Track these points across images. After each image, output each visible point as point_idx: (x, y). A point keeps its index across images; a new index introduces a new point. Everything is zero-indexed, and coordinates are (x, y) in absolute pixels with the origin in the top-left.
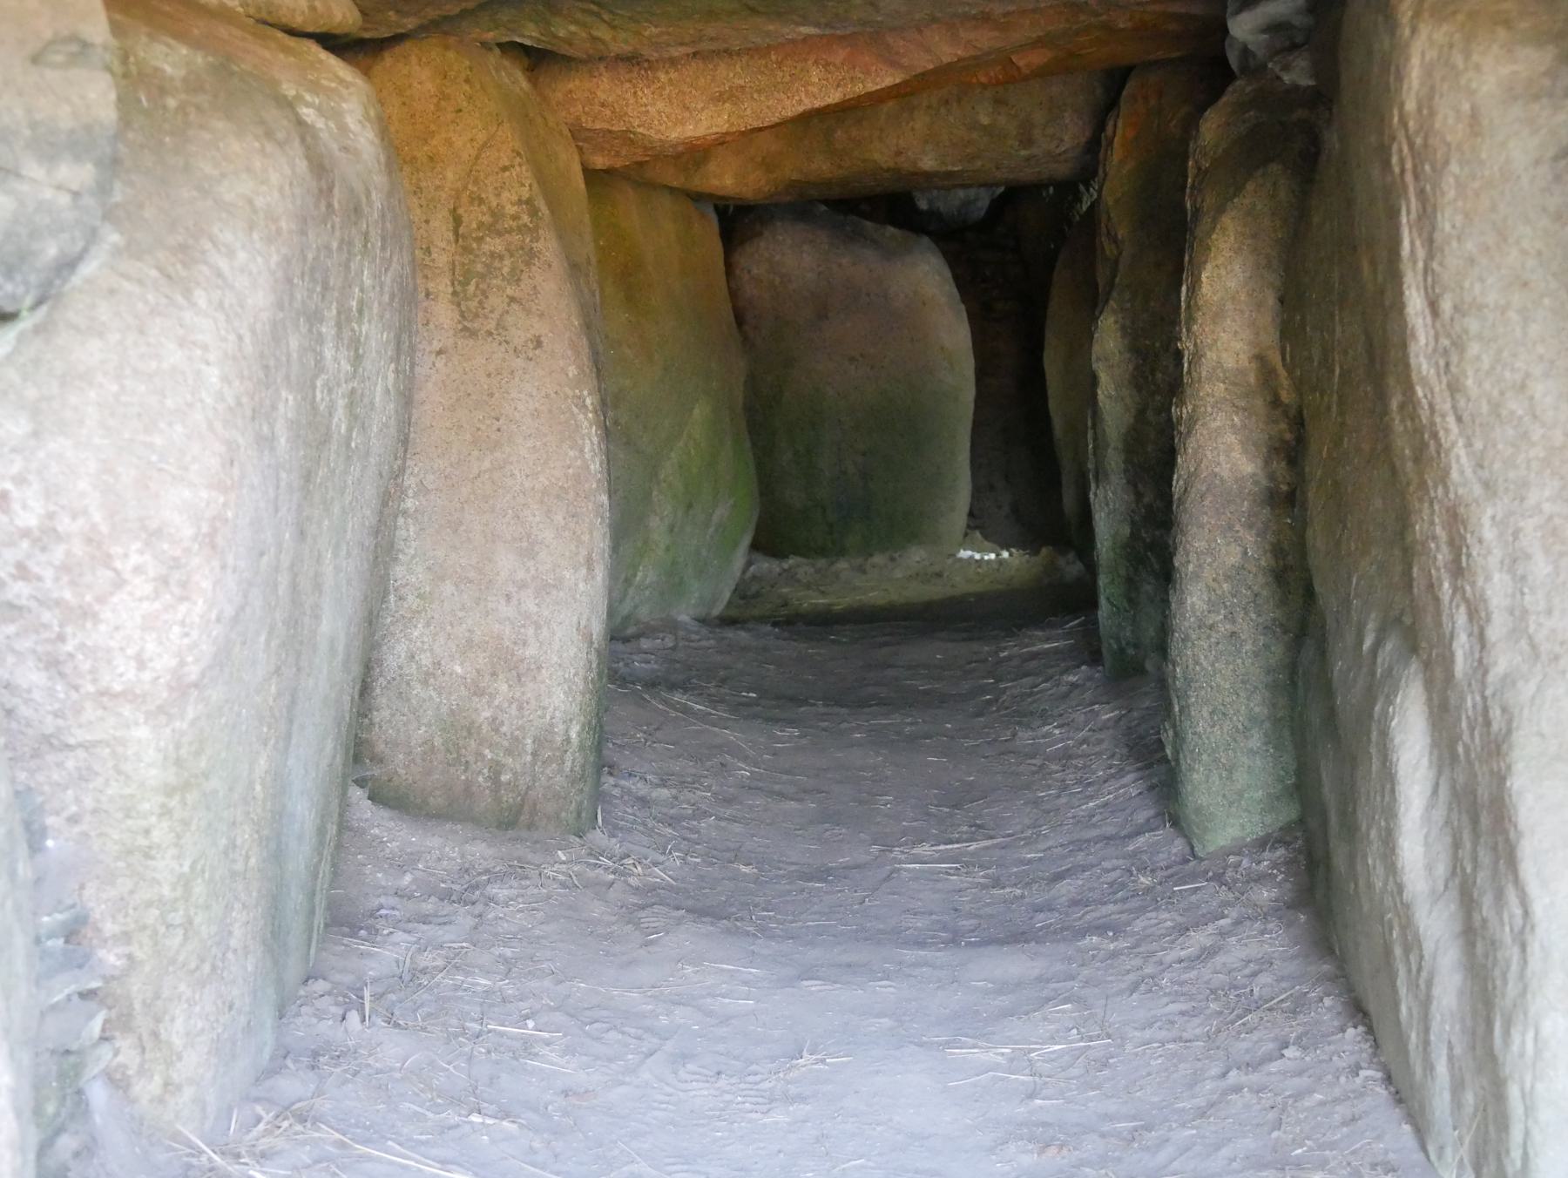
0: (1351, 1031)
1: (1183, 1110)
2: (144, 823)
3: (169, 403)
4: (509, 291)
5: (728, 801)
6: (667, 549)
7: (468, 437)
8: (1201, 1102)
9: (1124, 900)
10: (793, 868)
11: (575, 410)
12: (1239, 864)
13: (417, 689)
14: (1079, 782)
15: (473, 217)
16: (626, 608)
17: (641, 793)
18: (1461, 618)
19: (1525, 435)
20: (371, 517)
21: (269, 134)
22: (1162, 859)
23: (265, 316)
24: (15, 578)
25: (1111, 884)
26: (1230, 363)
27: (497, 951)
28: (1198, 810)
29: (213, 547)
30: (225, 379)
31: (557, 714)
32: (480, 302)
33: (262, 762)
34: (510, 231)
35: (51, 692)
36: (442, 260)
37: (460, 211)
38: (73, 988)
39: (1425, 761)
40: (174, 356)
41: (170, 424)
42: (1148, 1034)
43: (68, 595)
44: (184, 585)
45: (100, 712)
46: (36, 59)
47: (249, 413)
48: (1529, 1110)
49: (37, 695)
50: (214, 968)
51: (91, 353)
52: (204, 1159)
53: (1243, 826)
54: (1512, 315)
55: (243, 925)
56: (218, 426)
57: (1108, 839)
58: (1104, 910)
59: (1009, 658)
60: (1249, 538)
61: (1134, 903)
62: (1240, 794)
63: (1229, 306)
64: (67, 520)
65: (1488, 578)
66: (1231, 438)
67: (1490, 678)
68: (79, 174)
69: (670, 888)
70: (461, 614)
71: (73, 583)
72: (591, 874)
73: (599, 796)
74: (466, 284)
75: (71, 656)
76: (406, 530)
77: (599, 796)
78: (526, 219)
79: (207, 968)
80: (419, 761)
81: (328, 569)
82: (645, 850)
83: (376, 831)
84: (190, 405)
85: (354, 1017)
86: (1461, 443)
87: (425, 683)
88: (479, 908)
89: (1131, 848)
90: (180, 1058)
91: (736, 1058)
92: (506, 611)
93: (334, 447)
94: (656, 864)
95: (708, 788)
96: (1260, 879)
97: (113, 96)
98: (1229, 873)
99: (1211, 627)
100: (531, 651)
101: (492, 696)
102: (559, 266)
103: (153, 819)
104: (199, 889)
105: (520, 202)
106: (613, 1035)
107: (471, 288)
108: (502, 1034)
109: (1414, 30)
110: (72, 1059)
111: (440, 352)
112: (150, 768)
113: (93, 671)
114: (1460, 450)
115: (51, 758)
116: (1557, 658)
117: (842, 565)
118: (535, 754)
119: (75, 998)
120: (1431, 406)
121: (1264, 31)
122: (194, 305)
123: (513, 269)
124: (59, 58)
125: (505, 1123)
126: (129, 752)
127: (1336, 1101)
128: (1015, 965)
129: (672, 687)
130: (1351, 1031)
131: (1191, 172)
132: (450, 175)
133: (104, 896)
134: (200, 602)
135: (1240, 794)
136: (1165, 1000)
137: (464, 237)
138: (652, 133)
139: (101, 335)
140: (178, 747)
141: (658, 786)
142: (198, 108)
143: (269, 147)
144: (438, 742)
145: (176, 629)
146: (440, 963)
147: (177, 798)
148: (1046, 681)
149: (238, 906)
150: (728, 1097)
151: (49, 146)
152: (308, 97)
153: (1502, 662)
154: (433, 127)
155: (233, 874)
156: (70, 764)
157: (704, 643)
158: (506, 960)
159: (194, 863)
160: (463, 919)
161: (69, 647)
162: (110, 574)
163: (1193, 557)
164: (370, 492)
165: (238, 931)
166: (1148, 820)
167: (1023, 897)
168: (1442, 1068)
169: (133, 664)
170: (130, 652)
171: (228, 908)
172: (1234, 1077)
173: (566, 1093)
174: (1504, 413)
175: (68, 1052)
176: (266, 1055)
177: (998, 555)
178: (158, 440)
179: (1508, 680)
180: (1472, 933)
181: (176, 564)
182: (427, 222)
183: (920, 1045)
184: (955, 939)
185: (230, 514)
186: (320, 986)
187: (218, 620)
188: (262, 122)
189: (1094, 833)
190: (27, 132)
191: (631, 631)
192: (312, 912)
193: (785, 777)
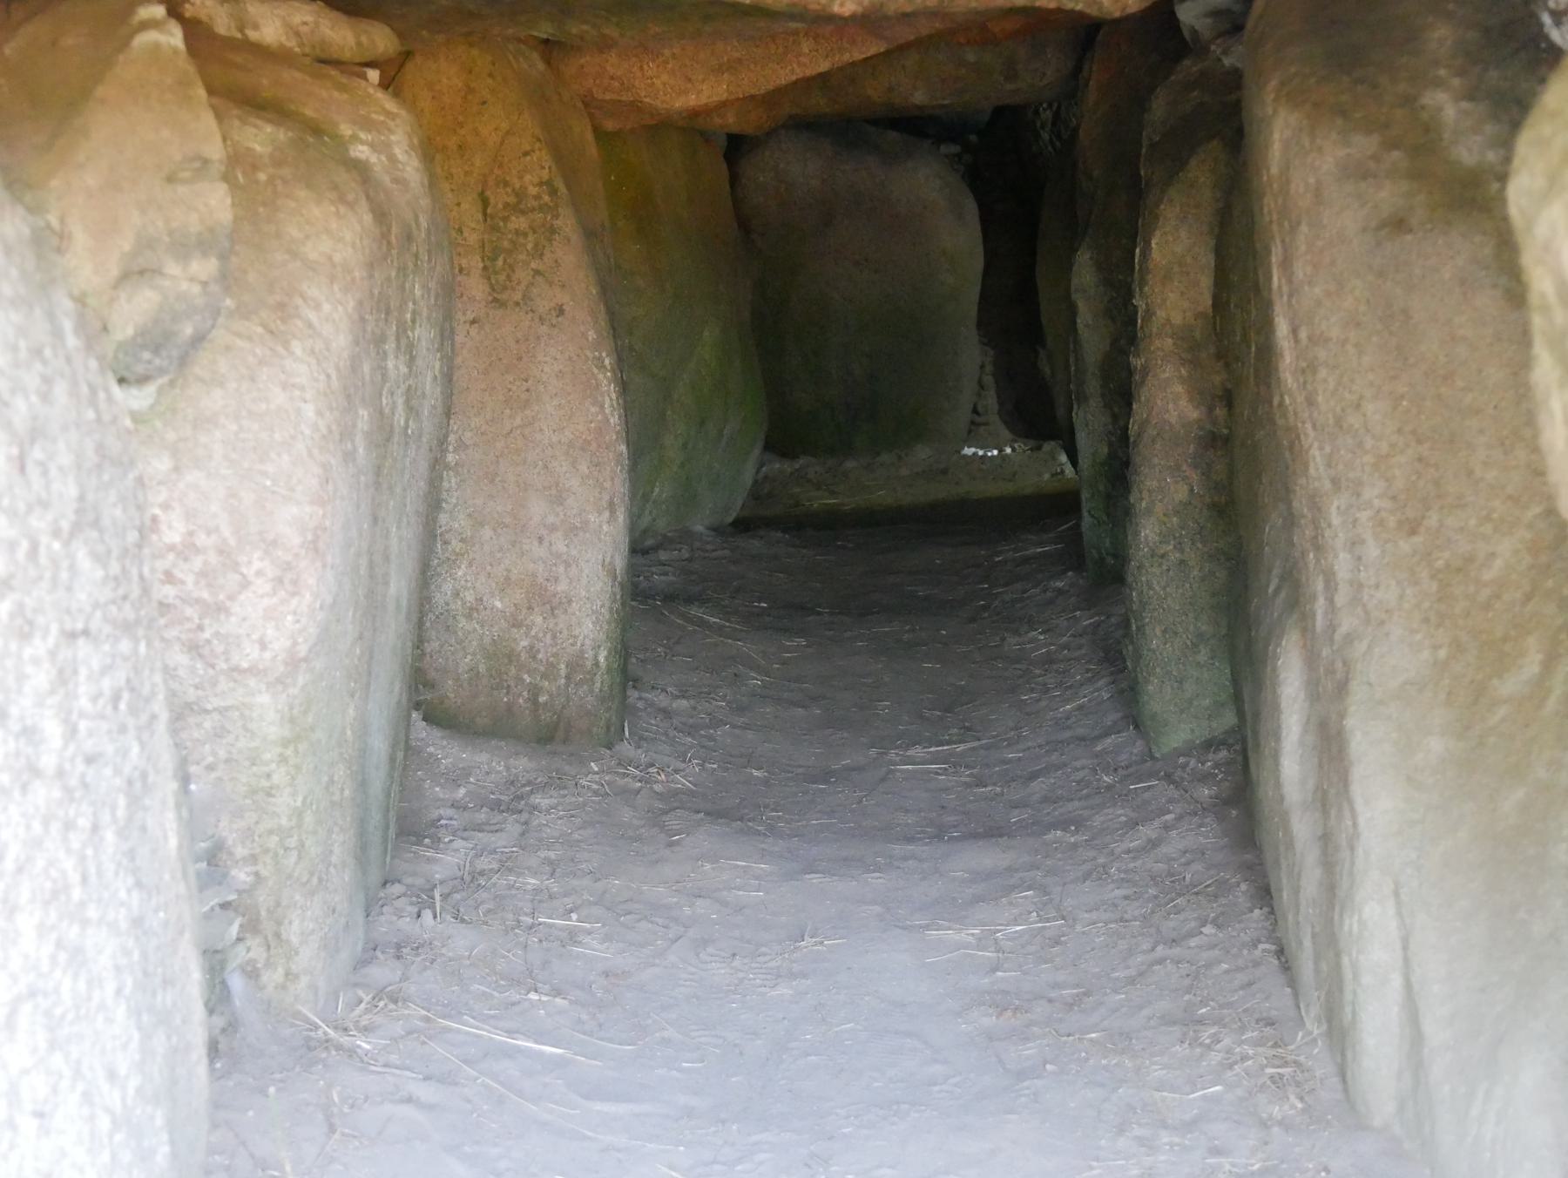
0: (1257, 911)
1: (1117, 979)
2: (266, 769)
3: (277, 436)
4: (533, 265)
5: (741, 709)
6: (682, 465)
7: (501, 398)
8: (1133, 972)
9: (1088, 797)
10: (800, 770)
11: (596, 371)
12: (1187, 764)
13: (463, 622)
14: (1059, 685)
15: (499, 198)
16: (645, 521)
17: (663, 705)
18: (1319, 585)
19: (1360, 445)
20: (424, 481)
21: (342, 199)
22: (1123, 758)
23: (345, 354)
24: (163, 583)
25: (1078, 782)
26: (1177, 319)
27: (542, 854)
28: (1154, 717)
29: (316, 550)
30: (319, 413)
31: (587, 642)
32: (508, 276)
33: (351, 712)
34: (533, 210)
35: (193, 670)
36: (473, 239)
37: (488, 193)
38: (216, 901)
39: (1302, 695)
40: (279, 398)
41: (279, 455)
42: (1094, 915)
43: (205, 595)
44: (295, 582)
45: (231, 685)
46: (171, 179)
47: (337, 437)
48: (1356, 976)
49: (181, 672)
50: (320, 880)
51: (215, 400)
52: (320, 1032)
53: (1192, 731)
54: (1350, 348)
55: (341, 845)
56: (316, 451)
57: (1083, 739)
58: (1070, 806)
59: (1005, 562)
60: (1195, 477)
61: (1097, 800)
62: (1190, 702)
63: (1176, 269)
64: (203, 537)
65: (1336, 556)
66: (1179, 388)
67: (1337, 637)
68: (204, 267)
69: (692, 794)
70: (499, 555)
71: (209, 585)
72: (621, 782)
73: (625, 710)
74: (494, 259)
75: (208, 642)
76: (450, 481)
77: (625, 710)
78: (546, 198)
79: (315, 880)
80: (465, 685)
81: (394, 542)
82: (666, 759)
83: (431, 749)
84: (293, 437)
85: (427, 915)
86: (1316, 445)
87: (469, 617)
88: (525, 816)
89: (1099, 748)
90: (297, 953)
91: (748, 942)
92: (539, 551)
93: (396, 439)
94: (676, 771)
95: (724, 698)
96: (1204, 778)
97: (229, 201)
98: (1179, 772)
99: (1163, 556)
100: (562, 587)
101: (529, 628)
102: (576, 238)
103: (274, 766)
104: (309, 818)
105: (541, 184)
106: (644, 925)
107: (500, 262)
108: (551, 926)
109: (1275, 111)
110: (219, 956)
111: (473, 322)
112: (272, 728)
113: (226, 652)
114: (1315, 452)
115: (192, 720)
116: (1382, 623)
117: (850, 464)
118: (568, 677)
119: (217, 909)
120: (1295, 414)
121: (1207, 15)
122: (292, 353)
123: (536, 245)
124: (187, 174)
125: (558, 1000)
126: (254, 715)
127: (1239, 969)
128: (987, 857)
129: (689, 600)
130: (1257, 911)
131: (1145, 142)
132: (478, 163)
133: (235, 826)
134: (308, 595)
135: (1190, 702)
136: (1111, 886)
137: (492, 217)
138: (658, 103)
139: (222, 385)
140: (291, 708)
141: (677, 697)
142: (285, 182)
143: (342, 209)
144: (482, 668)
145: (289, 618)
146: (495, 866)
147: (291, 748)
148: (1035, 587)
149: (336, 829)
150: (741, 975)
151: (183, 248)
152: (363, 136)
153: (1346, 624)
154: (461, 118)
155: (333, 803)
156: (207, 725)
157: (719, 553)
158: (550, 862)
159: (305, 798)
160: (512, 827)
161: (207, 635)
162: (237, 577)
163: (1145, 494)
164: (423, 466)
165: (337, 849)
166: (1115, 723)
167: (1002, 794)
168: (1307, 943)
169: (257, 646)
170: (254, 637)
171: (330, 831)
172: (1161, 950)
173: (606, 974)
174: (1345, 426)
175: (216, 952)
176: (360, 947)
177: (1000, 451)
178: (270, 468)
179: (1349, 639)
180: (1326, 839)
181: (288, 567)
182: (459, 204)
183: (904, 928)
184: (940, 834)
185: (328, 523)
186: (396, 889)
187: (321, 608)
188: (335, 187)
189: (1067, 734)
190: (167, 239)
191: (650, 542)
192: (387, 827)
193: (793, 685)
